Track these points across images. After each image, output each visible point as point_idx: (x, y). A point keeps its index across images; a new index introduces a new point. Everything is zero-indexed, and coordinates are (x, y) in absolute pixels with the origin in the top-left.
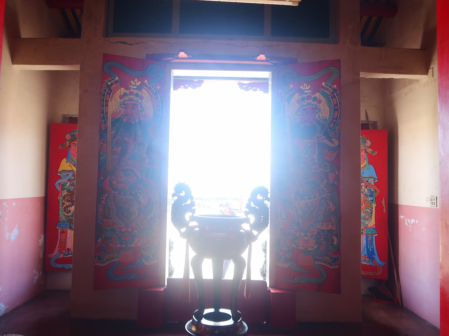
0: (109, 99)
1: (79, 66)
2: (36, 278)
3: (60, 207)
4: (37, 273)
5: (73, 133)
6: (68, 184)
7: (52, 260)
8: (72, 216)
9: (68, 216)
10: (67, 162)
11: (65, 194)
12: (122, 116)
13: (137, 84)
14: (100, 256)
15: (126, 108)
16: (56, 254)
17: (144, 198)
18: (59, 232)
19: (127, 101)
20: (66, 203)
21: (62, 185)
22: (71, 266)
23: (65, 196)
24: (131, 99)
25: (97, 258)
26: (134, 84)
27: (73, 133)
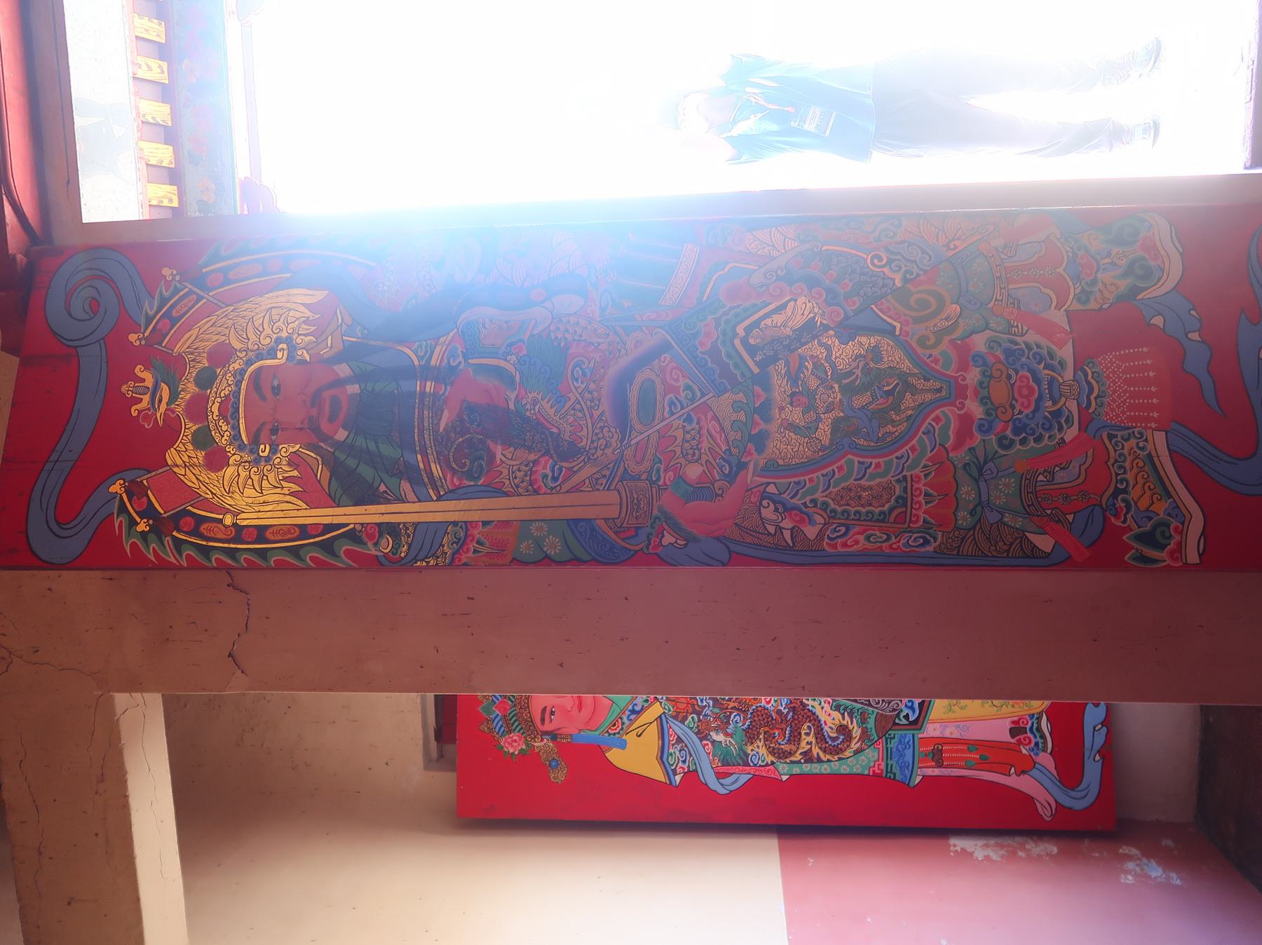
0: (228, 520)
1: (121, 699)
2: (1156, 871)
3: (824, 769)
4: (1130, 865)
5: (498, 724)
6: (720, 737)
7: (1066, 801)
8: (864, 720)
9: (865, 734)
10: (623, 745)
11: (763, 751)
12: (314, 448)
13: (149, 383)
14: (1141, 538)
15: (274, 431)
16: (1038, 785)
17: (783, 307)
18: (937, 772)
19: (236, 428)
20: (804, 747)
21: (725, 763)
22: (1093, 716)
23: (772, 752)
24: (228, 410)
25: (1155, 554)
26: (146, 399)
27: (498, 724)
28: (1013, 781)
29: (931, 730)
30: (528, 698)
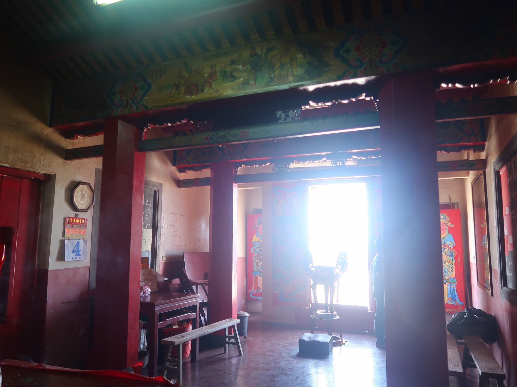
2: (243, 303)
22: (261, 298)
28: (253, 287)
29: (460, 370)
30: (161, 185)
